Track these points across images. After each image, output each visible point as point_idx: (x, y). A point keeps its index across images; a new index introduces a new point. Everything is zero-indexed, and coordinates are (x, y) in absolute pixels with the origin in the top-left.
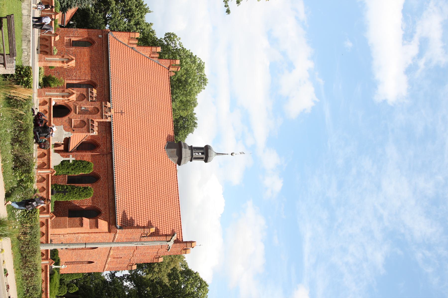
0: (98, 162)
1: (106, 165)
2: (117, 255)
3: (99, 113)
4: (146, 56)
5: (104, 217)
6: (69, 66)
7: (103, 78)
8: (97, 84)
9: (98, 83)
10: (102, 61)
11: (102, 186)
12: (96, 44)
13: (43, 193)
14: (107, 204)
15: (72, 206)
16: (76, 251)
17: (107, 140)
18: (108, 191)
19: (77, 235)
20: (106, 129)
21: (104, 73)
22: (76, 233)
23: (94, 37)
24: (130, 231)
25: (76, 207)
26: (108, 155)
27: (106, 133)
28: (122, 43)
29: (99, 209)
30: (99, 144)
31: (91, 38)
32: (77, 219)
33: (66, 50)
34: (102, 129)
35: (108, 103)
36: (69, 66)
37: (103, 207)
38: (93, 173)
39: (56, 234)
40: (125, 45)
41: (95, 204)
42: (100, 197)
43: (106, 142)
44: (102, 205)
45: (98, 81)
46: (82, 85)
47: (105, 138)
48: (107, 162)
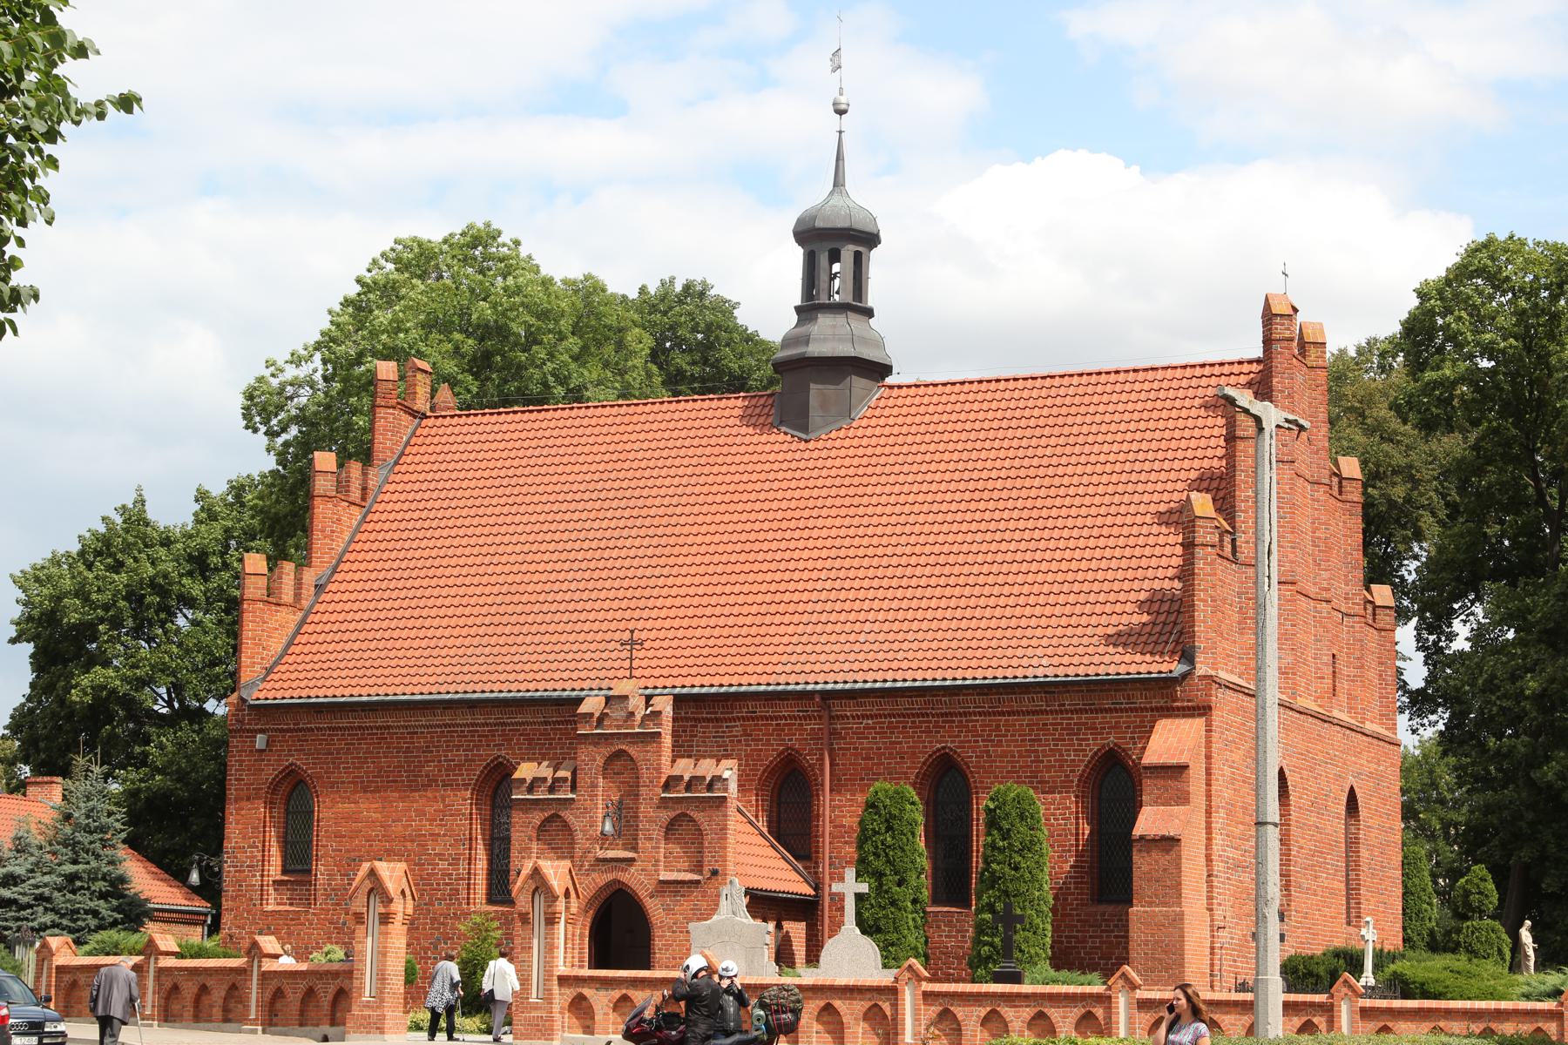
0: (868, 758)
3: (632, 751)
4: (360, 524)
6: (403, 892)
8: (492, 761)
9: (488, 754)
15: (1076, 888)
17: (762, 718)
18: (1009, 714)
19: (1218, 866)
20: (709, 720)
28: (294, 637)
29: (1092, 758)
30: (782, 752)
32: (1143, 864)
35: (583, 709)
40: (303, 622)
42: (1037, 751)
44: (1073, 745)
48: (868, 717)
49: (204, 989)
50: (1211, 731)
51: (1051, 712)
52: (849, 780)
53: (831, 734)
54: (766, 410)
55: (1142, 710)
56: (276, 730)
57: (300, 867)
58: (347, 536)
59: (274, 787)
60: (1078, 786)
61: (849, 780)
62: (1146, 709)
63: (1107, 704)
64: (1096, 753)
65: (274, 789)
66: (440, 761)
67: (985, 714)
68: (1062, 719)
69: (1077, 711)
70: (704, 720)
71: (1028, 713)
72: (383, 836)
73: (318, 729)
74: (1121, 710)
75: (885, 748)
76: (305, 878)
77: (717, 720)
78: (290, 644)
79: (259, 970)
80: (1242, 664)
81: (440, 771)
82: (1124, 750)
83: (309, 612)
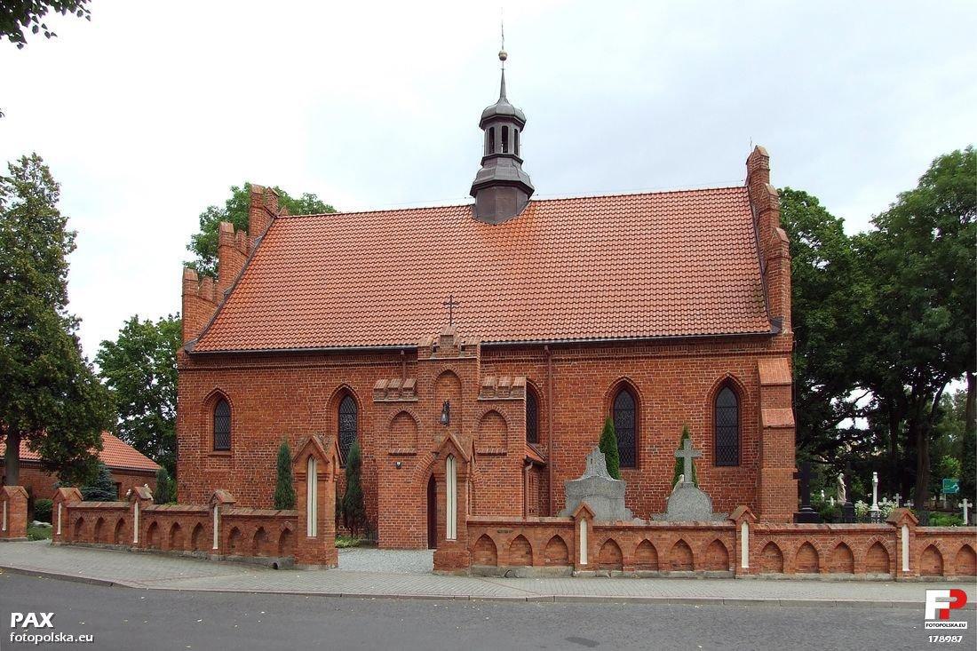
0: (575, 384)
3: (457, 371)
4: (246, 266)
9: (338, 381)
13: (821, 550)
17: (508, 361)
28: (214, 320)
40: (218, 313)
48: (575, 360)
51: (691, 356)
56: (207, 370)
57: (223, 447)
58: (240, 271)
59: (208, 401)
63: (726, 351)
64: (718, 381)
74: (735, 355)
76: (228, 453)
78: (212, 323)
79: (933, 574)
83: (221, 308)
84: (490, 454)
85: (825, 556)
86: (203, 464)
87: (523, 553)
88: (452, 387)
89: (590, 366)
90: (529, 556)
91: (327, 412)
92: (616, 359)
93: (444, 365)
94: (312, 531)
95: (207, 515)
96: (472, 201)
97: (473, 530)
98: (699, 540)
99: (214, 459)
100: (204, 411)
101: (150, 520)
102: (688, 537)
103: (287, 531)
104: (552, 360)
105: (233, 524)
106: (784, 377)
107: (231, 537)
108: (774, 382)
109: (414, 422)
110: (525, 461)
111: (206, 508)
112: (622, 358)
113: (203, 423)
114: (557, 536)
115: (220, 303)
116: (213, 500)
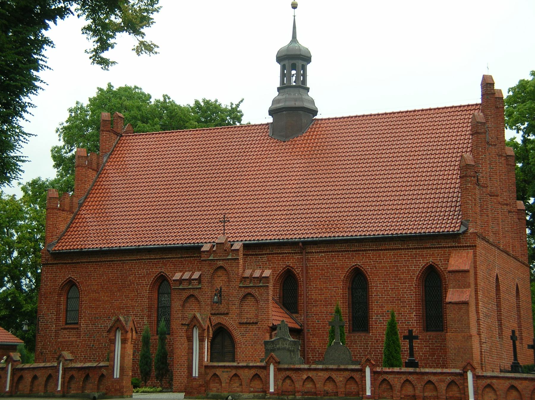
0: (322, 270)
1: (329, 255)
2: (504, 237)
3: (226, 266)
4: (96, 179)
5: (441, 260)
6: (132, 329)
7: (145, 262)
8: (158, 274)
9: (156, 270)
10: (110, 264)
11: (375, 262)
12: (72, 276)
14: (412, 252)
15: (417, 325)
16: (504, 319)
17: (276, 254)
18: (384, 250)
19: (481, 316)
20: (253, 255)
21: (135, 260)
22: (478, 317)
23: (57, 280)
24: (471, 205)
25: (419, 316)
26: (307, 251)
27: (262, 255)
28: (70, 225)
29: (422, 268)
30: (285, 268)
31: (61, 286)
32: (451, 315)
33: (86, 337)
34: (253, 262)
35: (203, 249)
36: (132, 329)
37: (418, 261)
38: (346, 280)
39: (482, 359)
40: (74, 218)
41: (412, 276)
42: (397, 266)
43: (281, 255)
44: (414, 263)
45: (151, 272)
46: (161, 304)
47: (271, 257)
48: (322, 252)
49: (35, 378)
50: (476, 256)
51: (403, 249)
52: (315, 279)
53: (306, 260)
54: (266, 130)
55: (444, 247)
56: (63, 263)
57: (73, 322)
58: (91, 183)
59: (62, 287)
60: (416, 280)
61: (315, 279)
62: (446, 247)
64: (424, 267)
65: (62, 289)
66: (135, 275)
67: (373, 250)
68: (408, 252)
69: (415, 248)
70: (251, 255)
71: (393, 249)
72: (110, 307)
73: (82, 262)
74: (435, 248)
75: (330, 266)
77: (256, 255)
78: (69, 227)
80: (482, 229)
81: (135, 279)
82: (436, 265)
84: (247, 323)
85: (419, 389)
86: (57, 335)
87: (238, 385)
88: (225, 278)
89: (332, 257)
90: (241, 387)
91: (149, 293)
92: (351, 251)
93: (218, 263)
94: (117, 374)
95: (56, 369)
96: (270, 120)
97: (208, 371)
98: (340, 377)
99: (65, 332)
100: (59, 295)
101: (18, 374)
102: (334, 375)
103: (103, 376)
104: (307, 253)
105: (71, 373)
106: (465, 265)
107: (69, 382)
108: (457, 269)
109: (199, 302)
110: (271, 327)
111: (56, 364)
112: (355, 251)
113: (59, 304)
114: (257, 374)
115: (75, 211)
116: (59, 359)
